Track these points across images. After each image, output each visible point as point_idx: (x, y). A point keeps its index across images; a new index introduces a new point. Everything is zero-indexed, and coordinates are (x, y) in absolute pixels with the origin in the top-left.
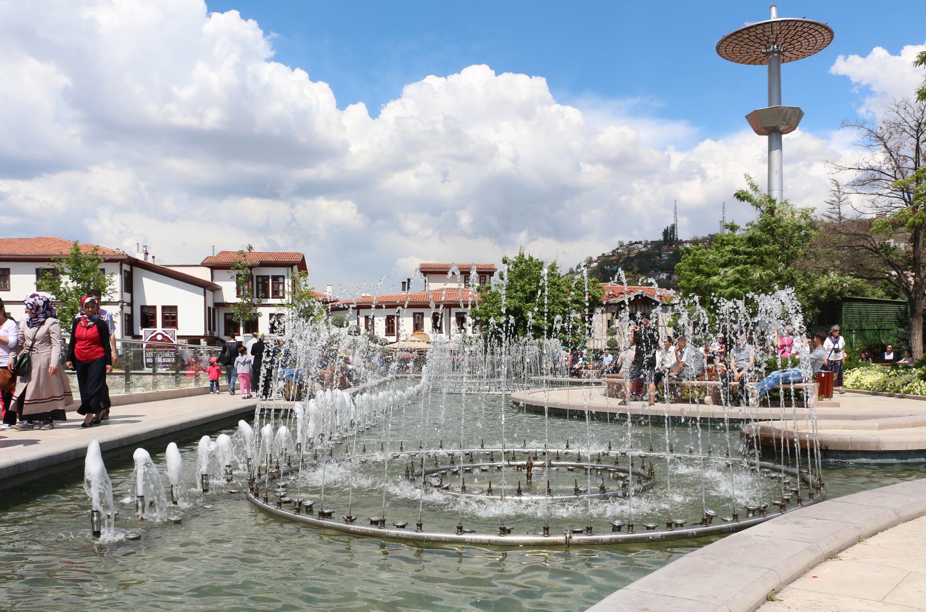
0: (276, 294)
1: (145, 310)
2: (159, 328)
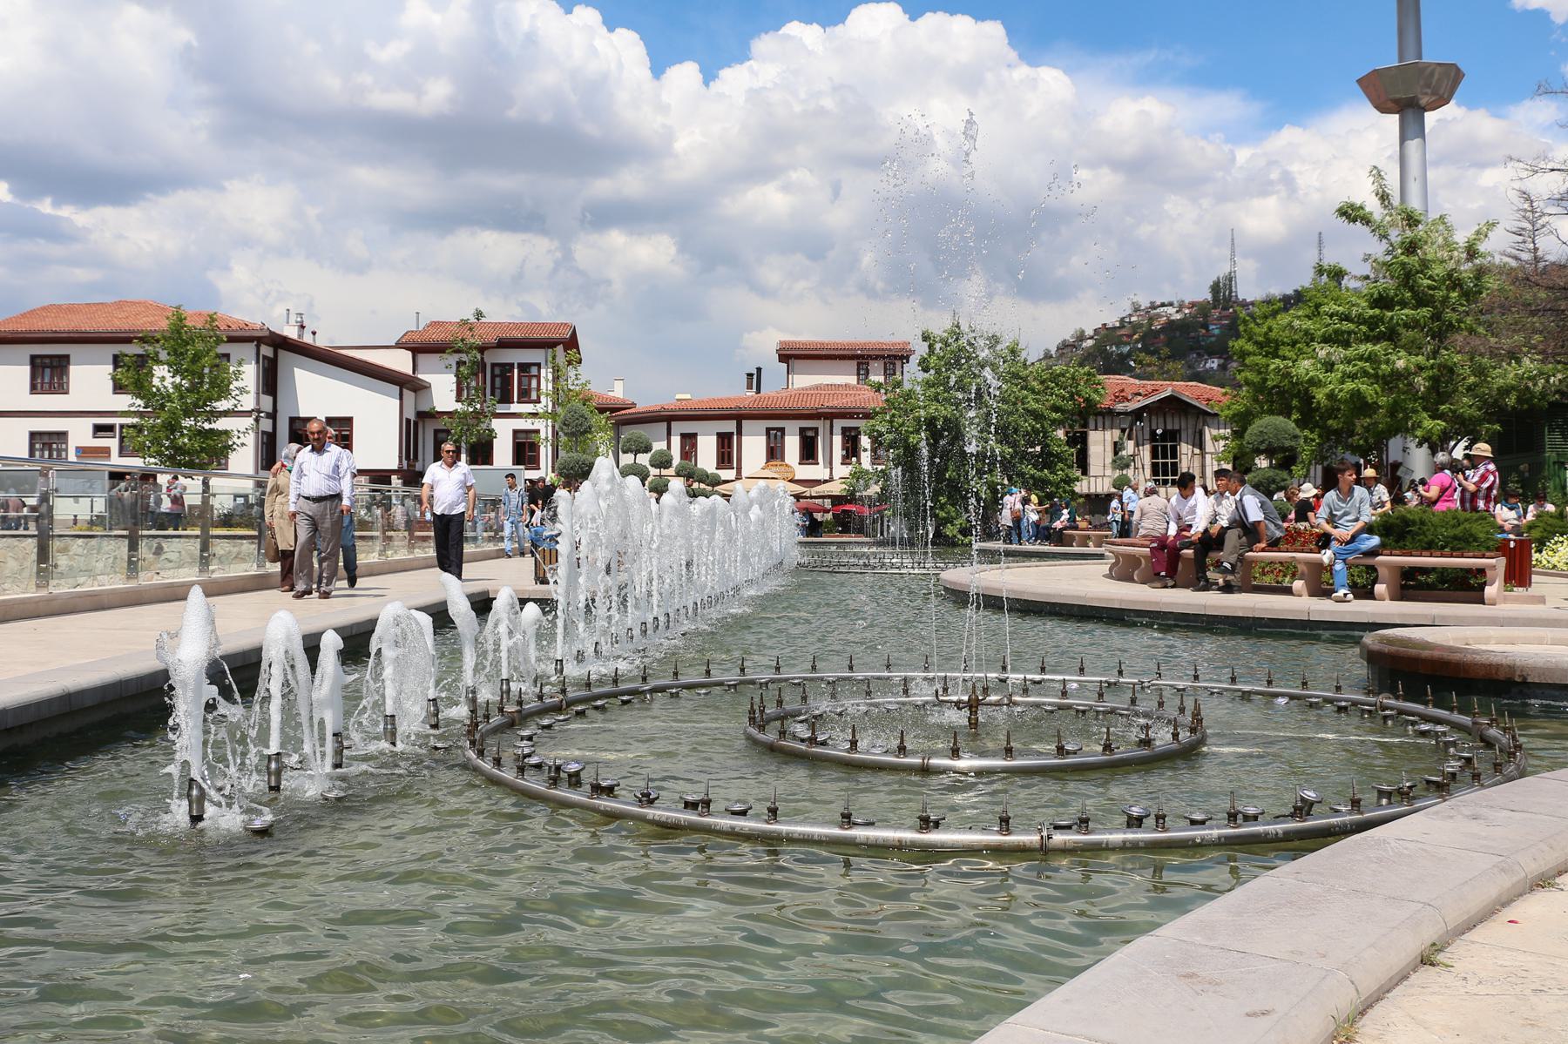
0: (525, 396)
1: (298, 425)
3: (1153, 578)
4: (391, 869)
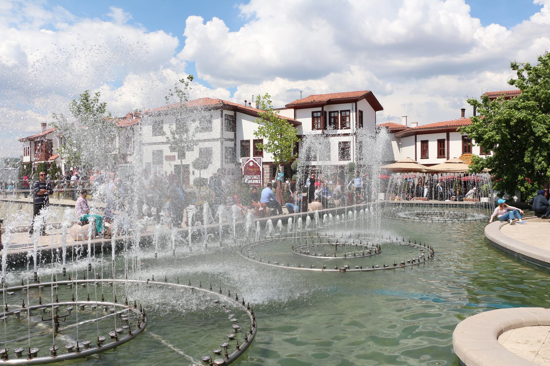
0: (343, 126)
1: (244, 144)
2: (252, 157)
3: (35, 282)
4: (180, 326)
